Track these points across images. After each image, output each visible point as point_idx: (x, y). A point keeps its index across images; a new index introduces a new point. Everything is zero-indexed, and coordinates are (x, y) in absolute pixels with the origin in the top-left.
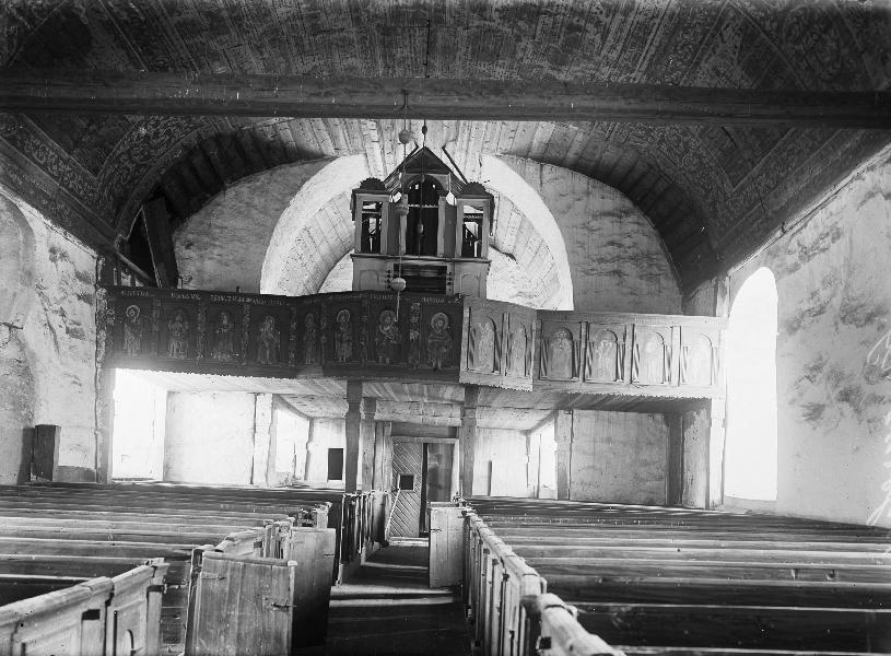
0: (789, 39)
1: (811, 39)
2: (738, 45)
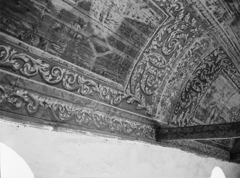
0: (151, 58)
2: (140, 20)
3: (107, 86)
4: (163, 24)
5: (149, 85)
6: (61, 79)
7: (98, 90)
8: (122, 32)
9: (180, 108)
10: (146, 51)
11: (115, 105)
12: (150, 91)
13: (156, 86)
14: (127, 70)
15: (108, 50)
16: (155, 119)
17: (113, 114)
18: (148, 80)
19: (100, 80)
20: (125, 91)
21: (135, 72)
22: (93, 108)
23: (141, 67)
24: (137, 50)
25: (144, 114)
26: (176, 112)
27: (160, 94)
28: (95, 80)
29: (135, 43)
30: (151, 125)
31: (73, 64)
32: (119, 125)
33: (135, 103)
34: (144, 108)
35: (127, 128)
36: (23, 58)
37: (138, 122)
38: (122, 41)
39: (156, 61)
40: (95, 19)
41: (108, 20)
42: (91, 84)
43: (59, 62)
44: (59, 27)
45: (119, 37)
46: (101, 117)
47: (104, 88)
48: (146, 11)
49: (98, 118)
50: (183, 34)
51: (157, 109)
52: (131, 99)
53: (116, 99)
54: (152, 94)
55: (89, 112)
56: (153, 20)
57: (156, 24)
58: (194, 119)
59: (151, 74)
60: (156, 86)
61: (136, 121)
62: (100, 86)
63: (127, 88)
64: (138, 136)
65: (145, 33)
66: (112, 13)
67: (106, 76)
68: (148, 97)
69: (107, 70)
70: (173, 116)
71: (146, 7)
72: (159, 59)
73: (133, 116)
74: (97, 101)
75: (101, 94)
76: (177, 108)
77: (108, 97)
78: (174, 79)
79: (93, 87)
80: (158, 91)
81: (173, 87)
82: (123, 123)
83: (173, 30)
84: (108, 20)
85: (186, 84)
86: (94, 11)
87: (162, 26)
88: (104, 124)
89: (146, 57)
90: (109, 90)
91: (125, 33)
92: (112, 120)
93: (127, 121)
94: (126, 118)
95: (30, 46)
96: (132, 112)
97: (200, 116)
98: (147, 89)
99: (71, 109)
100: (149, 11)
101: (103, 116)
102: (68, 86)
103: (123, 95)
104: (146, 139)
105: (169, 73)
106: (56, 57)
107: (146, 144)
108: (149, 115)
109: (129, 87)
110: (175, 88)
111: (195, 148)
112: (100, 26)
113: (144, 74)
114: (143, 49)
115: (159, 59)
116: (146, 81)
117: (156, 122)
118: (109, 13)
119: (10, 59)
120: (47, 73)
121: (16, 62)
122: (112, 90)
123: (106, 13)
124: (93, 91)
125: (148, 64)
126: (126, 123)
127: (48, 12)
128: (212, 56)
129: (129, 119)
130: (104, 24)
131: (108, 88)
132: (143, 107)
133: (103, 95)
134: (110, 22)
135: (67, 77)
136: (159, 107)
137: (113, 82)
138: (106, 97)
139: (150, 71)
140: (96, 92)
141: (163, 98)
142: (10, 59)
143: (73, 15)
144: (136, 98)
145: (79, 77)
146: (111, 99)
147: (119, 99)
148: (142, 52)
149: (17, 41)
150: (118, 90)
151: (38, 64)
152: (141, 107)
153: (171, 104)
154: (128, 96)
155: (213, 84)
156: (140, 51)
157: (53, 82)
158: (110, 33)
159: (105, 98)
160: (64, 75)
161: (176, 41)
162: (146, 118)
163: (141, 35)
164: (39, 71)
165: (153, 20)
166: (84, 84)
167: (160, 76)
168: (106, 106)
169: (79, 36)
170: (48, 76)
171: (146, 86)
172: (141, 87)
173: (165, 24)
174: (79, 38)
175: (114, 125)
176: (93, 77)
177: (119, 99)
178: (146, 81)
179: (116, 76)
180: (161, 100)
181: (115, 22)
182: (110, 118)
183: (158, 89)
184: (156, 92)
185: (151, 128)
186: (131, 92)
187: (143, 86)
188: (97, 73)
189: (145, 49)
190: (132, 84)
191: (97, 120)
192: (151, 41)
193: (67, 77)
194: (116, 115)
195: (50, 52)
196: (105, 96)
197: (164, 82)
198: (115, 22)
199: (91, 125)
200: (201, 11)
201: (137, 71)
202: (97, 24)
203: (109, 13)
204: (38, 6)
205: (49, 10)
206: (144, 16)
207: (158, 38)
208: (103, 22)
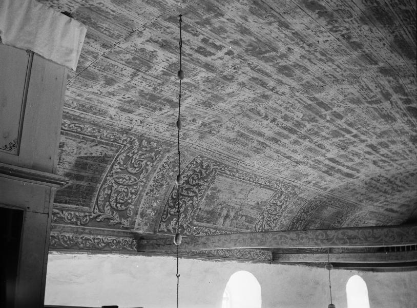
0: (116, 179)
1: (123, 189)
2: (93, 155)
3: (72, 211)
5: (121, 201)
7: (62, 216)
9: (169, 215)
11: (82, 225)
12: (123, 206)
13: (130, 201)
14: (92, 194)
16: (134, 231)
17: (82, 233)
18: (118, 198)
21: (102, 193)
22: (59, 231)
24: (99, 176)
25: (119, 228)
26: (163, 220)
27: (137, 207)
28: (57, 209)
29: (94, 172)
30: (130, 237)
32: (90, 242)
33: (106, 220)
34: (117, 223)
35: (98, 243)
37: (113, 236)
39: (124, 180)
41: (61, 162)
45: (76, 172)
46: (69, 237)
48: (98, 147)
49: (65, 239)
50: (147, 154)
51: (135, 221)
52: (101, 217)
54: (127, 209)
58: (195, 222)
59: (121, 192)
60: (130, 201)
62: (64, 212)
63: (94, 209)
64: (113, 250)
65: (163, 141)
67: (69, 203)
68: (121, 212)
70: (160, 225)
71: (97, 145)
72: (128, 178)
73: (106, 232)
74: (63, 225)
75: (66, 219)
76: (165, 216)
77: (74, 220)
78: (152, 191)
80: (134, 205)
81: (154, 198)
82: (94, 239)
83: (134, 153)
84: (61, 162)
85: (172, 192)
88: (72, 242)
89: (111, 180)
90: (74, 214)
92: (81, 238)
93: (99, 237)
94: (98, 235)
97: (204, 218)
98: (119, 205)
101: (71, 236)
103: (91, 215)
104: (123, 250)
105: (144, 187)
107: (122, 256)
108: (127, 228)
109: (96, 207)
110: (156, 198)
111: (203, 253)
115: (128, 178)
116: (117, 198)
117: (136, 233)
122: (77, 214)
124: (57, 217)
125: (114, 185)
126: (98, 239)
128: (194, 163)
129: (101, 235)
131: (73, 213)
136: (138, 219)
137: (77, 206)
140: (61, 218)
141: (142, 209)
147: (87, 220)
150: (85, 212)
152: (115, 223)
153: (155, 214)
155: (212, 186)
158: (66, 170)
161: (142, 161)
162: (122, 232)
163: (99, 165)
167: (133, 191)
171: (117, 203)
172: (110, 205)
173: (123, 151)
175: (84, 242)
177: (87, 220)
178: (117, 198)
179: (80, 201)
180: (139, 212)
182: (79, 236)
183: (133, 203)
184: (132, 206)
185: (131, 240)
186: (100, 211)
187: (113, 204)
188: (59, 203)
190: (99, 205)
191: (64, 241)
194: (87, 233)
197: (139, 196)
199: (58, 245)
200: (155, 137)
207: (119, 163)
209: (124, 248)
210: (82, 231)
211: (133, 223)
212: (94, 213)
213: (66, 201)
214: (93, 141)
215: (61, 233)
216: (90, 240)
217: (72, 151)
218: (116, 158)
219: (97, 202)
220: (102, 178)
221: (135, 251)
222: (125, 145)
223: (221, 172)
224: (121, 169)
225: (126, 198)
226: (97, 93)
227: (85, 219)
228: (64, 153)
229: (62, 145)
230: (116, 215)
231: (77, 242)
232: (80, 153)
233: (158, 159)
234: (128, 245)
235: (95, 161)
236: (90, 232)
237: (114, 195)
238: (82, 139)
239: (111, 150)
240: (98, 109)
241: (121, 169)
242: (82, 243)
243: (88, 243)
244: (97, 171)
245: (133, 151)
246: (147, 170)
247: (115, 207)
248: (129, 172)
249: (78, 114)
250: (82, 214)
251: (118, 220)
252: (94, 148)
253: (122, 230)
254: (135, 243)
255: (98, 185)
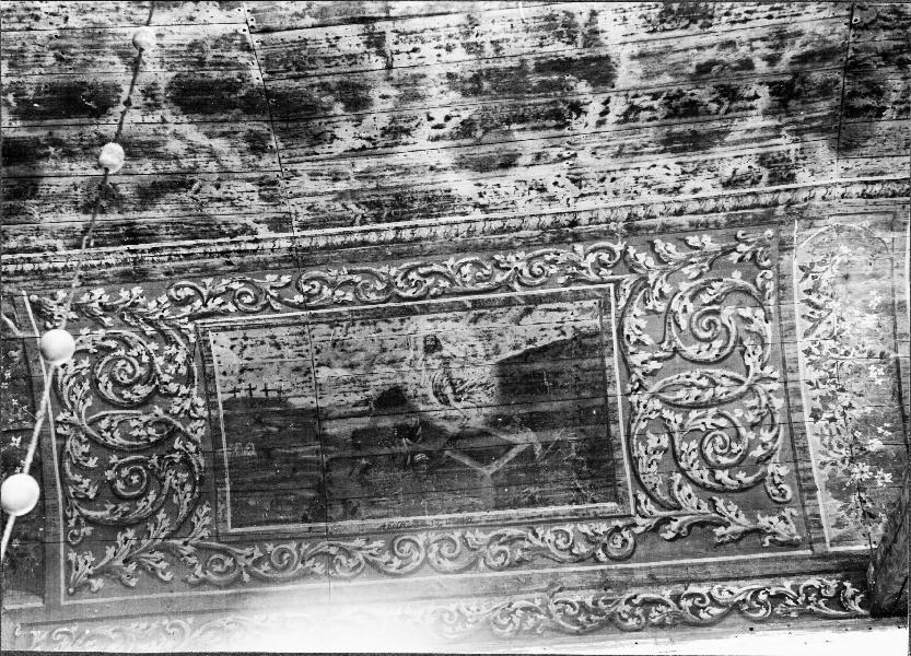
2: (539, 344)
4: (617, 306)
5: (724, 460)
6: (422, 556)
7: (537, 542)
8: (517, 391)
10: (629, 390)
15: (510, 446)
17: (624, 585)
18: (709, 452)
19: (533, 517)
20: (633, 512)
23: (648, 432)
24: (600, 401)
25: (762, 549)
29: (578, 393)
31: (437, 517)
34: (746, 533)
35: (695, 610)
36: (325, 549)
38: (534, 409)
40: (435, 411)
41: (462, 392)
42: (510, 537)
43: (403, 525)
44: (367, 465)
45: (518, 407)
47: (556, 531)
48: (537, 315)
51: (818, 516)
52: (675, 525)
53: (611, 545)
54: (760, 481)
55: (538, 603)
56: (575, 321)
57: (597, 321)
59: (708, 431)
61: (737, 579)
62: (540, 531)
63: (638, 502)
66: (456, 375)
69: (538, 489)
71: (529, 311)
75: (553, 550)
79: (521, 542)
82: (677, 598)
84: (462, 392)
86: (416, 397)
87: (620, 315)
88: (593, 617)
91: (527, 391)
92: (628, 601)
93: (693, 589)
94: (686, 582)
95: (330, 525)
96: (700, 557)
99: (478, 610)
100: (543, 313)
101: (589, 601)
102: (447, 565)
103: (635, 525)
106: (391, 520)
109: (642, 497)
112: (455, 413)
113: (677, 443)
114: (615, 391)
115: (704, 382)
118: (450, 379)
119: (303, 562)
120: (386, 557)
121: (315, 562)
123: (445, 382)
124: (523, 550)
125: (667, 414)
127: (330, 452)
129: (699, 582)
130: (458, 405)
132: (740, 529)
133: (561, 550)
134: (471, 393)
135: (435, 547)
138: (574, 551)
139: (690, 424)
142: (303, 562)
143: (379, 429)
144: (690, 517)
145: (468, 535)
146: (597, 549)
147: (625, 541)
148: (619, 398)
149: (304, 526)
151: (360, 549)
152: (734, 534)
154: (655, 521)
156: (610, 400)
157: (408, 568)
158: (485, 411)
159: (572, 554)
160: (427, 546)
164: (366, 559)
165: (575, 321)
166: (488, 545)
167: (751, 418)
168: (587, 572)
169: (418, 457)
170: (392, 563)
172: (692, 481)
174: (421, 461)
176: (508, 520)
178: (703, 456)
181: (481, 385)
186: (662, 506)
189: (623, 388)
190: (649, 487)
192: (624, 360)
193: (435, 547)
195: (373, 517)
196: (570, 548)
198: (481, 385)
200: (679, 213)
201: (642, 448)
202: (442, 414)
203: (450, 379)
204: (307, 453)
205: (332, 448)
206: (543, 329)
208: (452, 402)
209: (803, 614)
210: (623, 578)
211: (813, 522)
212: (644, 517)
213: (532, 498)
214: (509, 303)
215: (552, 596)
216: (663, 603)
217: (471, 352)
218: (620, 330)
219: (635, 475)
220: (615, 404)
221: (858, 616)
222: (617, 283)
223: (870, 196)
224: (658, 359)
225: (736, 448)
226: (364, 148)
227: (619, 540)
228: (454, 365)
229: (432, 346)
230: (728, 508)
231: (613, 614)
232: (497, 351)
233: (771, 286)
234: (821, 603)
235: (555, 358)
236: (651, 576)
237: (688, 447)
238: (474, 308)
239: (584, 311)
240: (420, 196)
241: (658, 359)
242: (633, 616)
243: (654, 614)
244: (583, 387)
245: (656, 293)
246: (760, 338)
247: (706, 480)
248: (694, 361)
249: (391, 235)
250: (603, 528)
251: (743, 522)
252: (527, 320)
253: (773, 555)
254: (850, 591)
255: (613, 427)
